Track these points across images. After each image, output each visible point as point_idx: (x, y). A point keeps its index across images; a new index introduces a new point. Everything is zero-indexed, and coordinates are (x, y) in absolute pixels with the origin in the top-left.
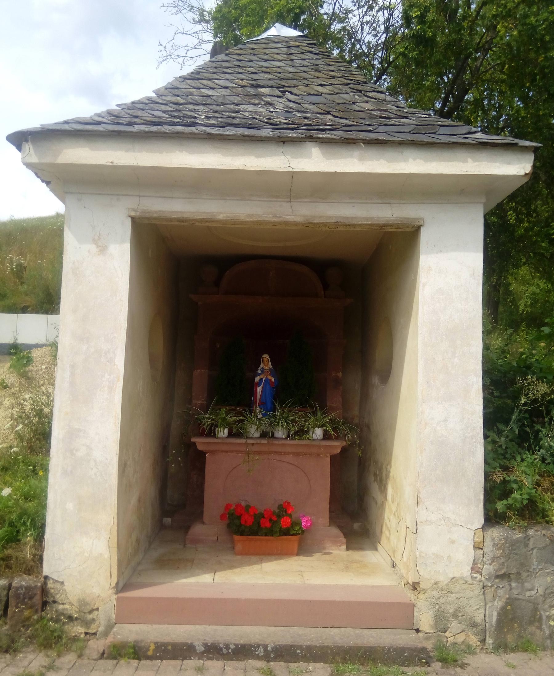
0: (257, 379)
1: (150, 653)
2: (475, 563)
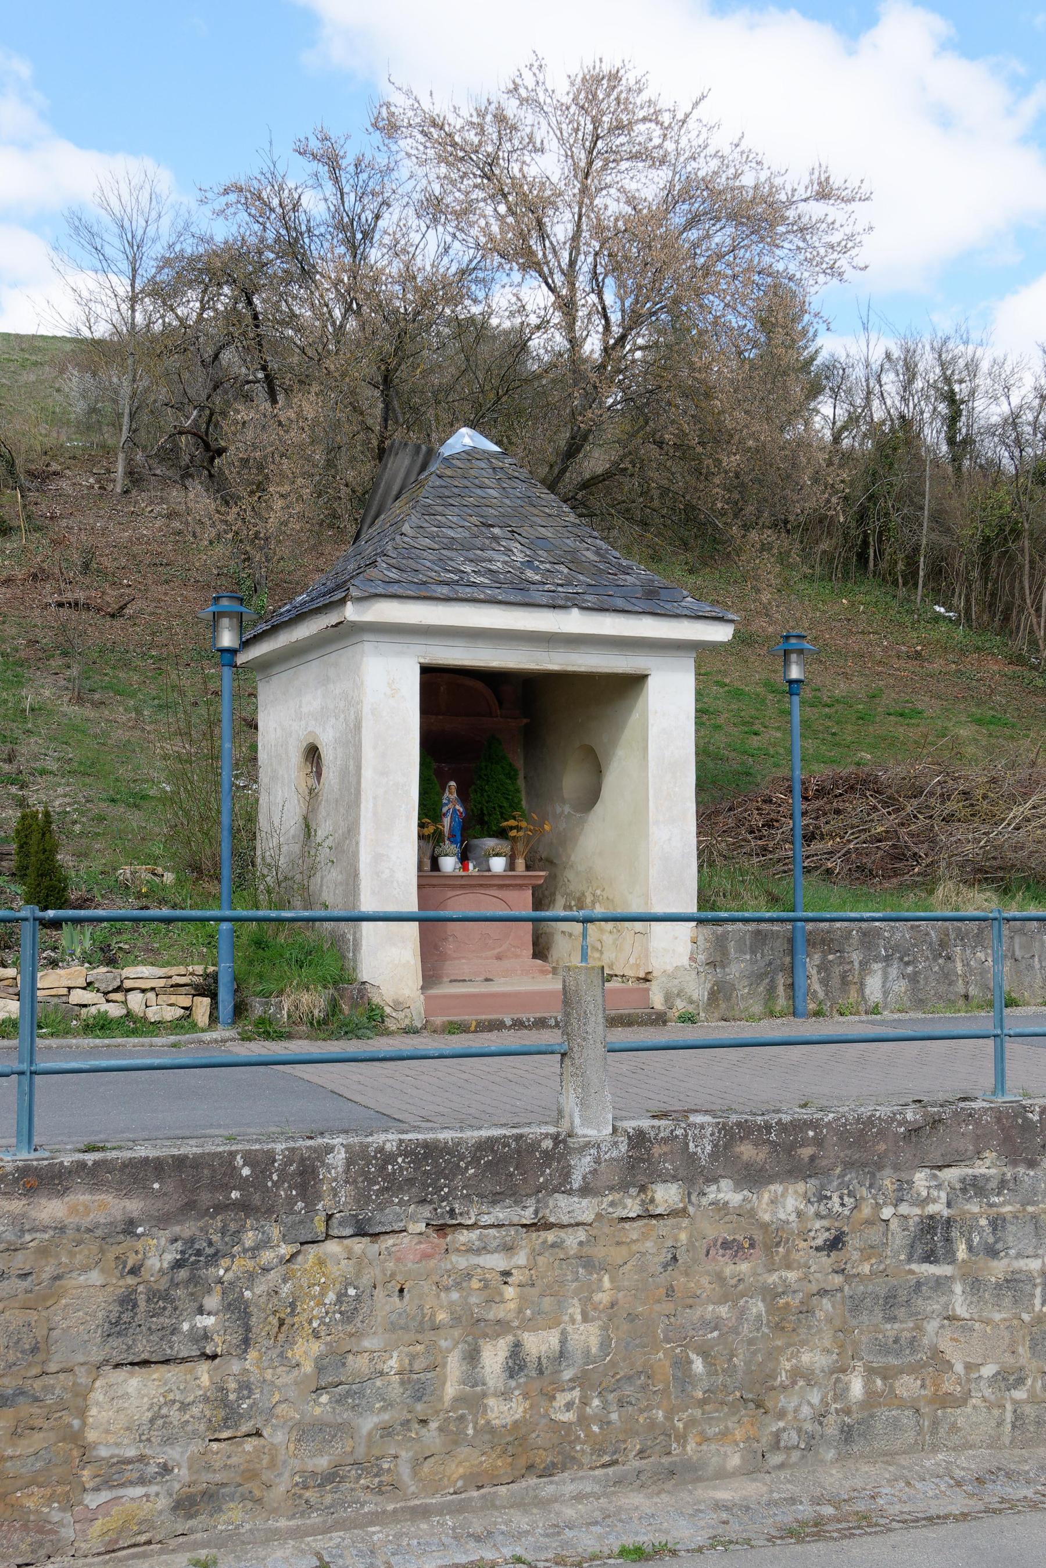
0: (444, 810)
1: (473, 1029)
2: (692, 953)
